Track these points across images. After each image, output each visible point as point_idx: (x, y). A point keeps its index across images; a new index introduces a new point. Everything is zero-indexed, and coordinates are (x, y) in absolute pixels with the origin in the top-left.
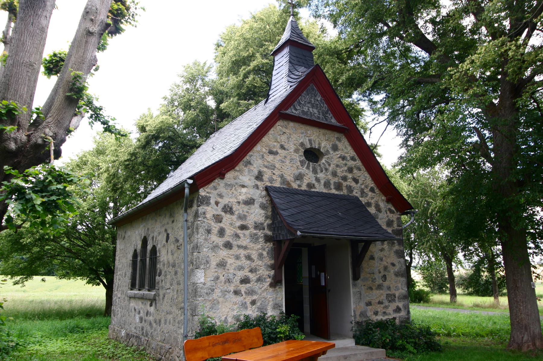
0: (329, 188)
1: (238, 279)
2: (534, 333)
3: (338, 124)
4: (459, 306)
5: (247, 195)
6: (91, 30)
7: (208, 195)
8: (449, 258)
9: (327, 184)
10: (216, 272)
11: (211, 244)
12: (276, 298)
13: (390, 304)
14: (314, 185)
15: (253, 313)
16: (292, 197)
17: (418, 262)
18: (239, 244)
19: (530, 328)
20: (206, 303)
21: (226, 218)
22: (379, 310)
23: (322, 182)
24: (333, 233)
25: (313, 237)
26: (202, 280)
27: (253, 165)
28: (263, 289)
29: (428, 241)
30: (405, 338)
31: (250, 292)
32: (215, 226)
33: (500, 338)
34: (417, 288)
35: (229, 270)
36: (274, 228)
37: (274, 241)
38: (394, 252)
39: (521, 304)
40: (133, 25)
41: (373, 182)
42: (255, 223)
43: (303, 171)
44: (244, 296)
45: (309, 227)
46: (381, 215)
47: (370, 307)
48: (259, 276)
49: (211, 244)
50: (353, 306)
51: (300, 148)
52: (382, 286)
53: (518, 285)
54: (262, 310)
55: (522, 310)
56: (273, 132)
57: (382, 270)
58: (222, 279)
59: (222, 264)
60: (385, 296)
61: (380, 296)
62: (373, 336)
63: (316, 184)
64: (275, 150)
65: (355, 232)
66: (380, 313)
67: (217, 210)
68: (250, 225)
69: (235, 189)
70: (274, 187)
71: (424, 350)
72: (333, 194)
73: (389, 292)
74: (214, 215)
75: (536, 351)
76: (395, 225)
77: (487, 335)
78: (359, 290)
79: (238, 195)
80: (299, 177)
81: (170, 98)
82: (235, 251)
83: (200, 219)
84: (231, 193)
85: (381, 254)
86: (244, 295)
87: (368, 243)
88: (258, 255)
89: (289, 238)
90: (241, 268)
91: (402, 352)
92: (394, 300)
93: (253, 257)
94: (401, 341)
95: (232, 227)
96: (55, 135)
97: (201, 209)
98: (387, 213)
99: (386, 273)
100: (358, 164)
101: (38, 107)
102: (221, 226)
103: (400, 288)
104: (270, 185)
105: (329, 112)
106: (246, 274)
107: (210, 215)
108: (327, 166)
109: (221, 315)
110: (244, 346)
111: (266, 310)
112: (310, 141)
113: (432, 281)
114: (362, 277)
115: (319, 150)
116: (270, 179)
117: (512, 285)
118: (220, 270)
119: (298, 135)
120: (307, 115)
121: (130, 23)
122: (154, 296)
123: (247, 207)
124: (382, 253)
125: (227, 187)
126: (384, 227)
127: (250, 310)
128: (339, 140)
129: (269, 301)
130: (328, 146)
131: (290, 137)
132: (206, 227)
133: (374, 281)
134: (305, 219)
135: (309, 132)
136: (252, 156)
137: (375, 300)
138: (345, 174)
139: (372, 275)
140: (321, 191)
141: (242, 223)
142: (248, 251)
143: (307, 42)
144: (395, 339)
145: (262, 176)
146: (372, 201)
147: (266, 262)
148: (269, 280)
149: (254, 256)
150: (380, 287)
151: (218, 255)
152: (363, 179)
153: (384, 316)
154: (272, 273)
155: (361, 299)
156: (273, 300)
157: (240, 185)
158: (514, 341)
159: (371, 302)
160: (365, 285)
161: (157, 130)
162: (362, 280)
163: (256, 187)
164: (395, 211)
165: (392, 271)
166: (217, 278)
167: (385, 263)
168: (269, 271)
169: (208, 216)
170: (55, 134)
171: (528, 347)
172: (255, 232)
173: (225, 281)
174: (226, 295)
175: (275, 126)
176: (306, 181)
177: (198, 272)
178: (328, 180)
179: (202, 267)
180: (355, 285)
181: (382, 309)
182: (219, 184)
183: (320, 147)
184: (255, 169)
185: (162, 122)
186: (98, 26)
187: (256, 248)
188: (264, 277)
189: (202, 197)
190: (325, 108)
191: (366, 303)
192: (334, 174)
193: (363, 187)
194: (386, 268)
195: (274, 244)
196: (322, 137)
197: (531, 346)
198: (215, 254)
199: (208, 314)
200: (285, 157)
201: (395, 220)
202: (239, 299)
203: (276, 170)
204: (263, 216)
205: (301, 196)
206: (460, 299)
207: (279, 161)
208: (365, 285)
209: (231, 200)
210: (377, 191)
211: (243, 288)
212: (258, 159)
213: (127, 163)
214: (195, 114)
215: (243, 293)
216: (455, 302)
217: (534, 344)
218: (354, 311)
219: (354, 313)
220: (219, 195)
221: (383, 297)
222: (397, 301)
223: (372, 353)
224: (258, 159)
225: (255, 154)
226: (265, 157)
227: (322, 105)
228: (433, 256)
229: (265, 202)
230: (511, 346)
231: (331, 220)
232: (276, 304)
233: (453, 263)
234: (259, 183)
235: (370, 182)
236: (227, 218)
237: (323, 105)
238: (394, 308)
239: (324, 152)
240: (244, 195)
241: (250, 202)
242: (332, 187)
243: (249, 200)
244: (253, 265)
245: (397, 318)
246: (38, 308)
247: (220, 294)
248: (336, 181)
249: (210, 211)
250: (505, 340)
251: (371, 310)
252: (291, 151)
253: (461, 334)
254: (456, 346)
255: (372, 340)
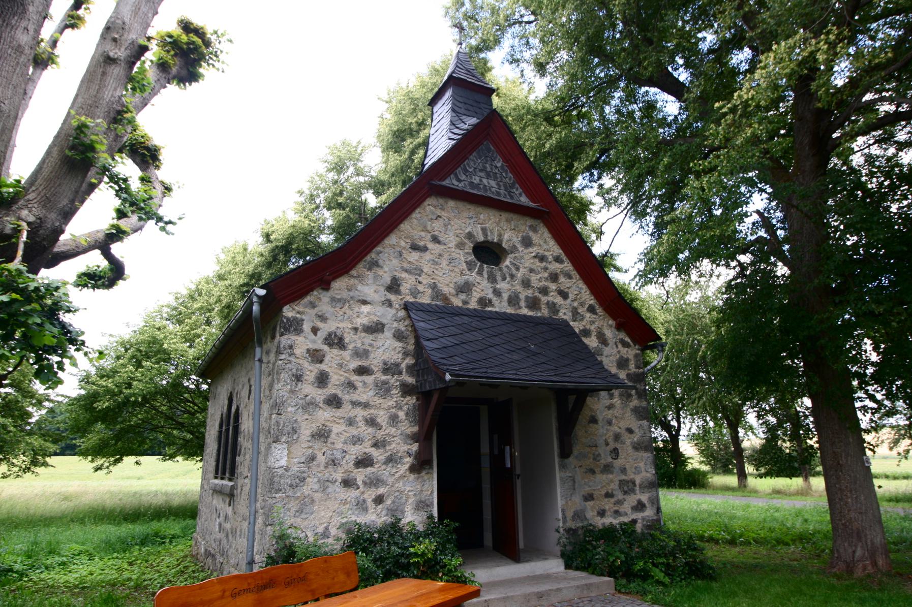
0: (517, 306)
1: (351, 458)
2: (873, 543)
3: (531, 204)
4: (750, 492)
5: (372, 317)
6: (111, 54)
7: (298, 316)
8: (735, 420)
9: (513, 300)
10: (310, 447)
11: (301, 399)
12: (422, 491)
13: (625, 497)
14: (490, 301)
15: (376, 518)
16: (450, 319)
17: (690, 429)
18: (354, 400)
19: (866, 536)
20: (288, 503)
21: (332, 355)
22: (607, 508)
23: (505, 296)
24: (514, 377)
25: (482, 384)
26: (283, 462)
27: (382, 267)
28: (397, 475)
29: (700, 398)
30: (651, 557)
31: (373, 482)
32: (310, 368)
33: (815, 547)
34: (690, 467)
35: (334, 443)
36: (418, 371)
37: (419, 393)
38: (632, 410)
39: (849, 495)
40: (218, 69)
41: (593, 298)
42: (385, 364)
43: (471, 279)
44: (362, 488)
45: (470, 366)
46: (607, 350)
47: (591, 503)
48: (390, 453)
49: (301, 399)
50: (560, 502)
51: (466, 241)
52: (612, 466)
53: (841, 462)
54: (395, 512)
55: (851, 504)
56: (419, 215)
57: (610, 441)
58: (321, 459)
59: (322, 435)
60: (617, 483)
61: (608, 484)
62: (593, 555)
63: (495, 300)
64: (422, 244)
65: (556, 375)
66: (608, 513)
67: (314, 342)
68: (375, 366)
69: (350, 307)
70: (420, 304)
71: (683, 577)
72: (525, 316)
73: (624, 477)
74: (308, 350)
75: (879, 576)
76: (632, 366)
77: (794, 541)
78: (570, 475)
79: (355, 316)
80: (465, 288)
81: (307, 192)
82: (347, 410)
83: (283, 357)
84: (341, 313)
85: (609, 414)
86: (361, 486)
87: (582, 394)
88: (390, 418)
89: (438, 387)
90: (357, 440)
91: (643, 583)
92: (633, 491)
93: (379, 420)
94: (642, 564)
95: (343, 370)
96: (38, 221)
97: (285, 340)
98: (617, 347)
99: (618, 446)
100: (567, 269)
101: (18, 178)
102: (321, 368)
103: (643, 469)
104: (412, 300)
105: (517, 185)
106: (367, 450)
107: (300, 350)
108: (514, 271)
109: (318, 523)
110: (313, 592)
111: (403, 512)
112: (484, 230)
113: (712, 455)
114: (575, 452)
115: (499, 245)
116: (413, 291)
117: (831, 462)
118: (318, 445)
119: (464, 221)
120: (479, 189)
121: (213, 66)
122: (231, 490)
123: (371, 337)
124: (611, 411)
125: (334, 303)
126: (614, 370)
127: (373, 513)
128: (534, 229)
129: (408, 497)
130: (515, 239)
131: (449, 224)
132: (294, 371)
133: (598, 458)
134: (466, 355)
135: (482, 216)
136: (381, 252)
137: (601, 492)
138: (544, 283)
139: (593, 448)
140: (503, 311)
141: (360, 363)
142: (372, 411)
143: (482, 82)
144: (632, 558)
145: (399, 286)
146: (592, 328)
147: (403, 428)
148: (408, 461)
149: (382, 418)
150: (607, 469)
151: (314, 417)
152: (576, 293)
153: (615, 518)
154: (415, 447)
155: (574, 489)
156: (415, 495)
157: (359, 301)
158: (839, 557)
159: (593, 494)
160: (581, 466)
161: (288, 238)
162: (576, 457)
163: (389, 304)
164: (631, 343)
165: (628, 442)
166: (313, 458)
167: (616, 429)
168: (408, 444)
169: (297, 351)
170: (40, 219)
171: (865, 568)
172: (384, 378)
173: (327, 463)
174: (327, 487)
175: (422, 206)
176: (476, 295)
177: (275, 448)
178: (515, 293)
179: (283, 440)
180: (563, 467)
181: (612, 506)
182: (320, 299)
183: (501, 240)
184: (385, 275)
185: (294, 226)
186: (126, 49)
187: (386, 406)
188: (400, 454)
189: (288, 319)
190: (510, 179)
191: (583, 496)
192: (526, 284)
193: (576, 304)
194: (617, 437)
195: (418, 399)
196: (504, 225)
197: (870, 568)
198: (309, 417)
199: (292, 521)
200: (440, 255)
201: (631, 357)
202: (352, 494)
203: (424, 276)
204: (399, 352)
205: (465, 318)
206: (752, 481)
207: (429, 262)
208: (581, 466)
209: (341, 325)
210: (599, 310)
211: (360, 475)
212: (392, 258)
213: (245, 289)
214: (344, 215)
215: (360, 483)
216: (745, 486)
217: (875, 564)
218: (563, 511)
219: (564, 514)
220: (319, 316)
221: (614, 486)
222: (638, 492)
223: (588, 586)
224: (392, 258)
225: (387, 250)
226: (405, 255)
227: (504, 174)
228: (711, 420)
229: (403, 329)
230: (834, 567)
231: (516, 357)
232: (421, 502)
233: (740, 430)
234: (392, 297)
235: (588, 297)
236: (332, 355)
237: (506, 174)
238: (634, 504)
239: (507, 248)
240: (366, 316)
241: (376, 328)
242: (523, 304)
243: (374, 325)
244: (380, 435)
245: (639, 521)
246: (130, 503)
247: (316, 487)
248: (530, 295)
249: (302, 343)
250: (823, 551)
251: (592, 508)
252: (451, 245)
253: (752, 541)
254: (742, 563)
255: (592, 562)
